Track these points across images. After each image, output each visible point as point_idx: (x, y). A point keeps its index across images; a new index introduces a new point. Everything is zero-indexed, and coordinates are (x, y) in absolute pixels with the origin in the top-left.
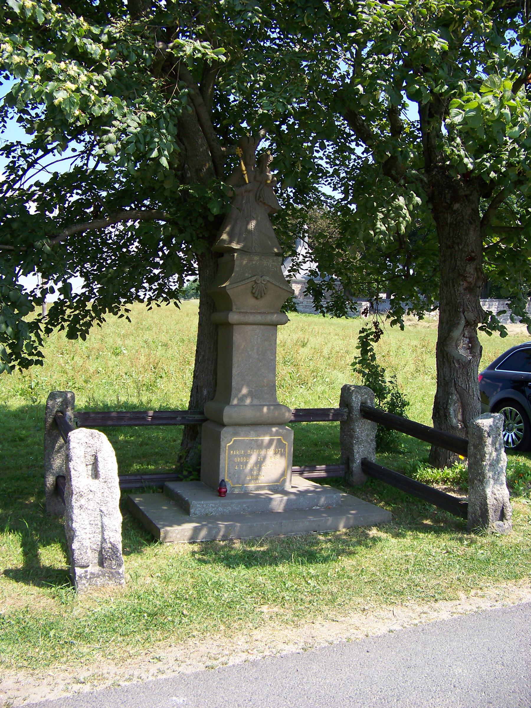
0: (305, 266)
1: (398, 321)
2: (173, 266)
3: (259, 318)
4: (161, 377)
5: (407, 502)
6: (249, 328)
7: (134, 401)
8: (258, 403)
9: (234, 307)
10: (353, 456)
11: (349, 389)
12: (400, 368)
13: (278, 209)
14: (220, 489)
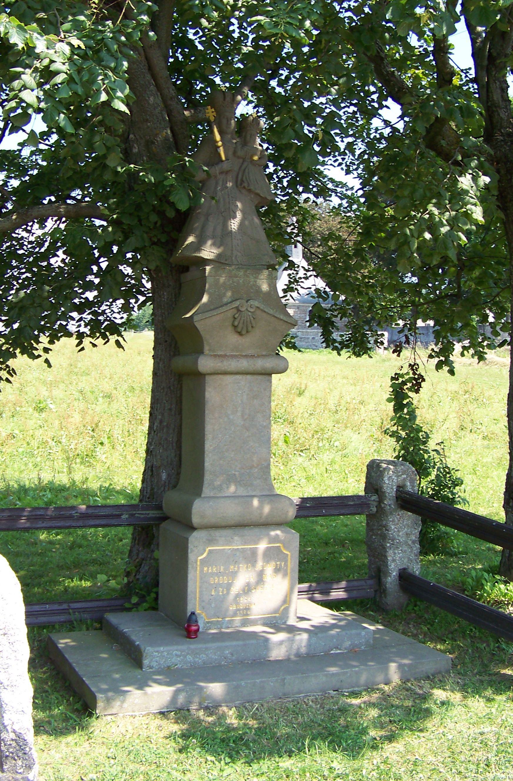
0: (307, 284)
1: (444, 362)
2: (113, 286)
3: (244, 364)
4: (102, 444)
5: (471, 637)
6: (229, 379)
7: (63, 479)
8: (245, 493)
9: (206, 348)
10: (387, 566)
11: (378, 466)
12: (438, 425)
13: (269, 198)
14: (189, 626)
